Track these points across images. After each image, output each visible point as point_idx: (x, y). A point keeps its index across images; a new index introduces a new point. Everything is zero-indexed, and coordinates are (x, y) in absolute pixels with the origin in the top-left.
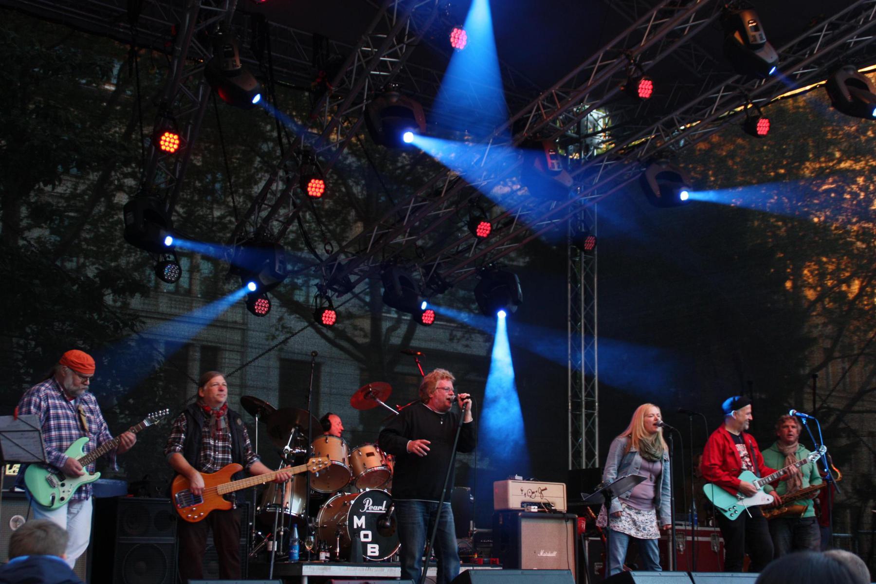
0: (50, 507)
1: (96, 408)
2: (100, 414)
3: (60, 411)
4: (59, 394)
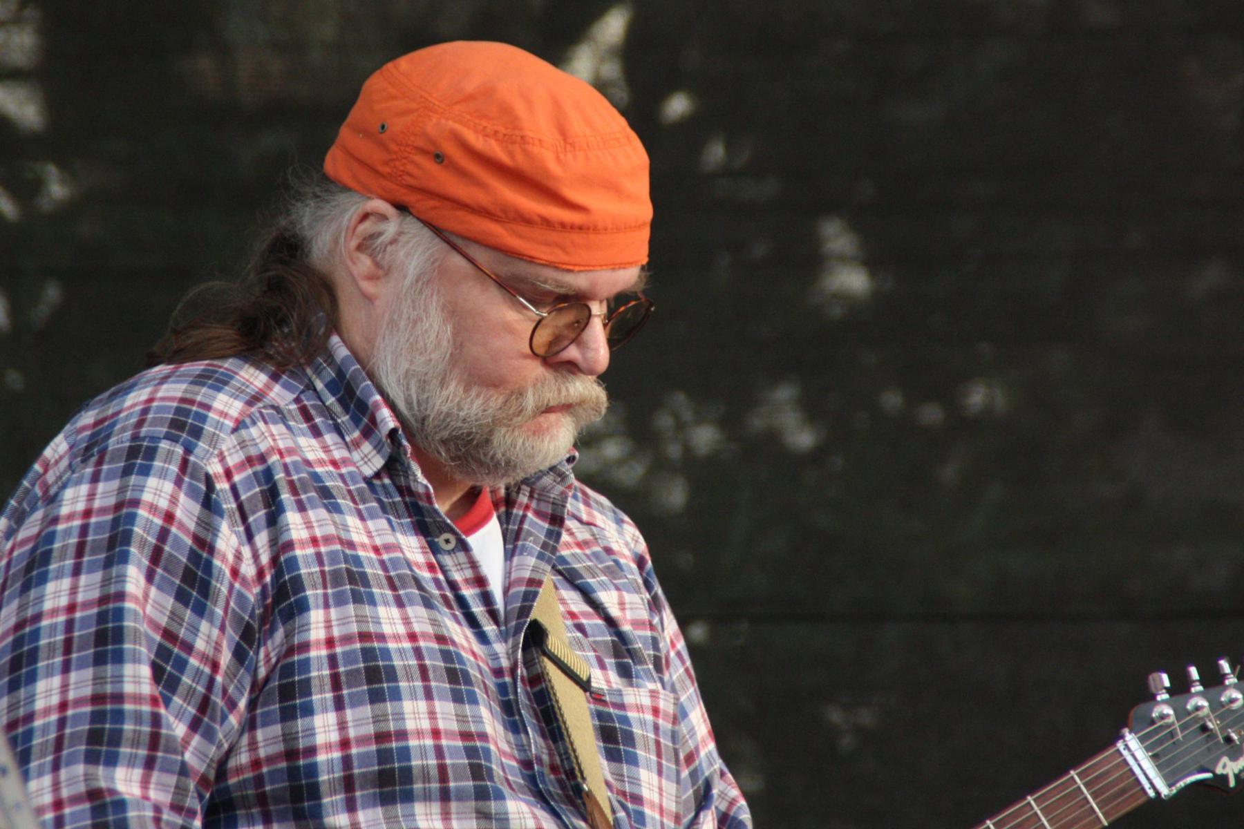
3: (388, 619)
4: (370, 461)
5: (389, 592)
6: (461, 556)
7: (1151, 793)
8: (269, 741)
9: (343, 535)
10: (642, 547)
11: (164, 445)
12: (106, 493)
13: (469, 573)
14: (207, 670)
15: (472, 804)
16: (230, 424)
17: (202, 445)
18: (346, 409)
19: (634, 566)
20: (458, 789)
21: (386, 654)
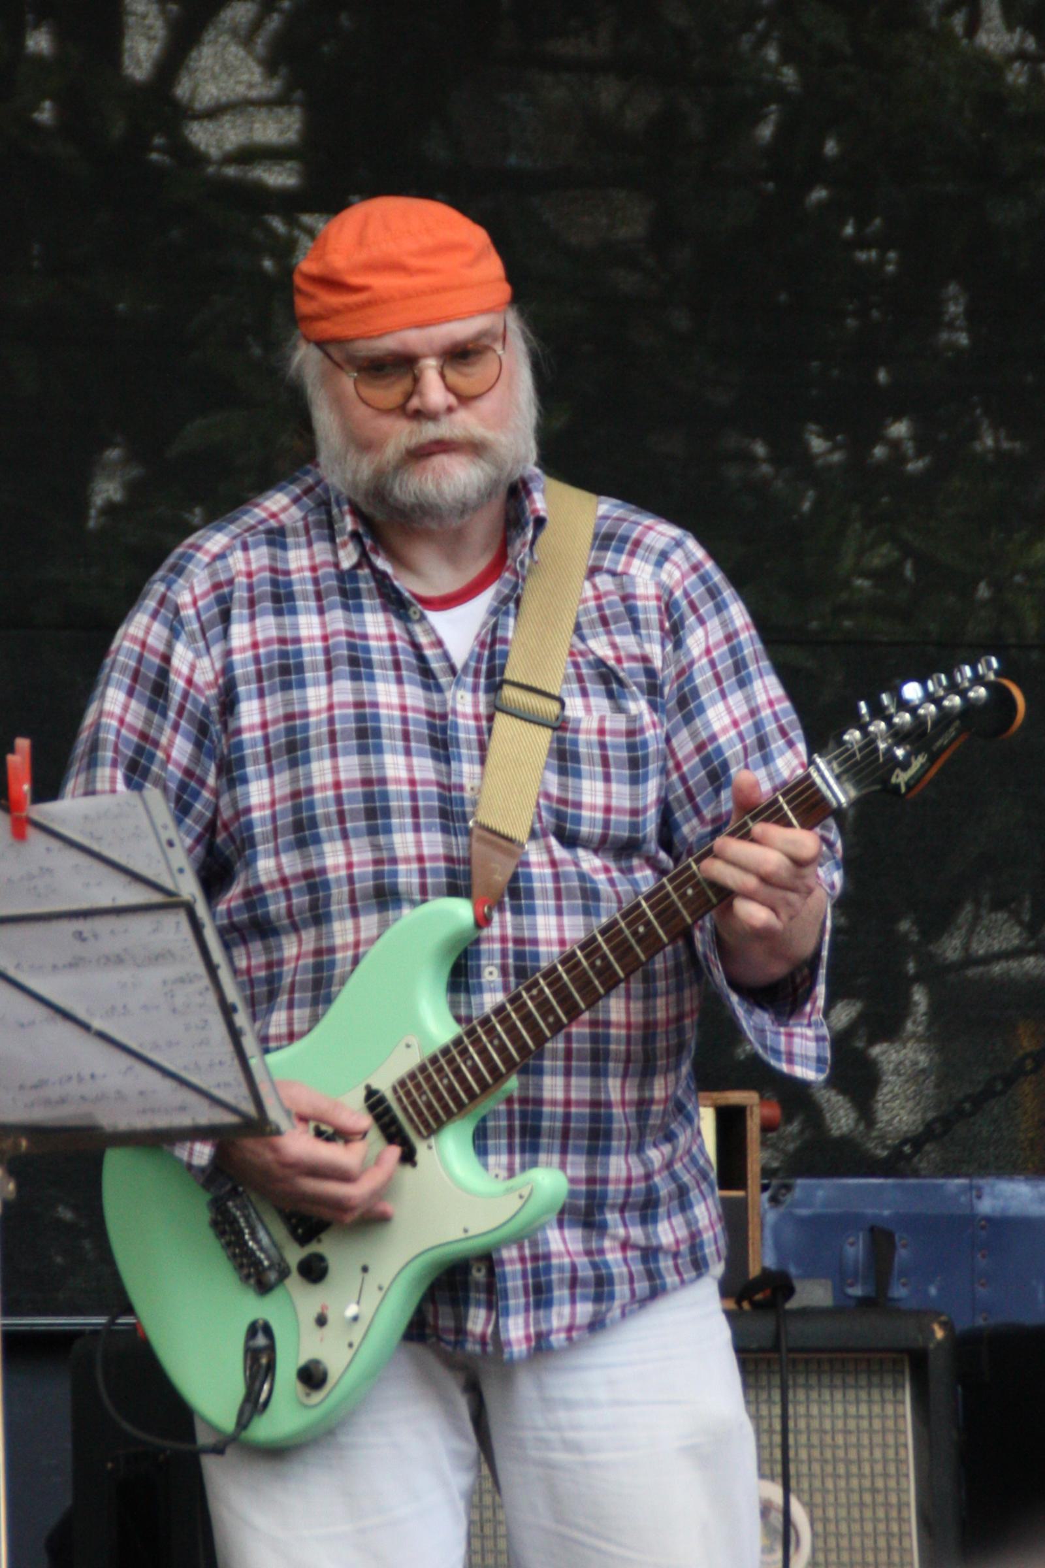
7: (834, 804)
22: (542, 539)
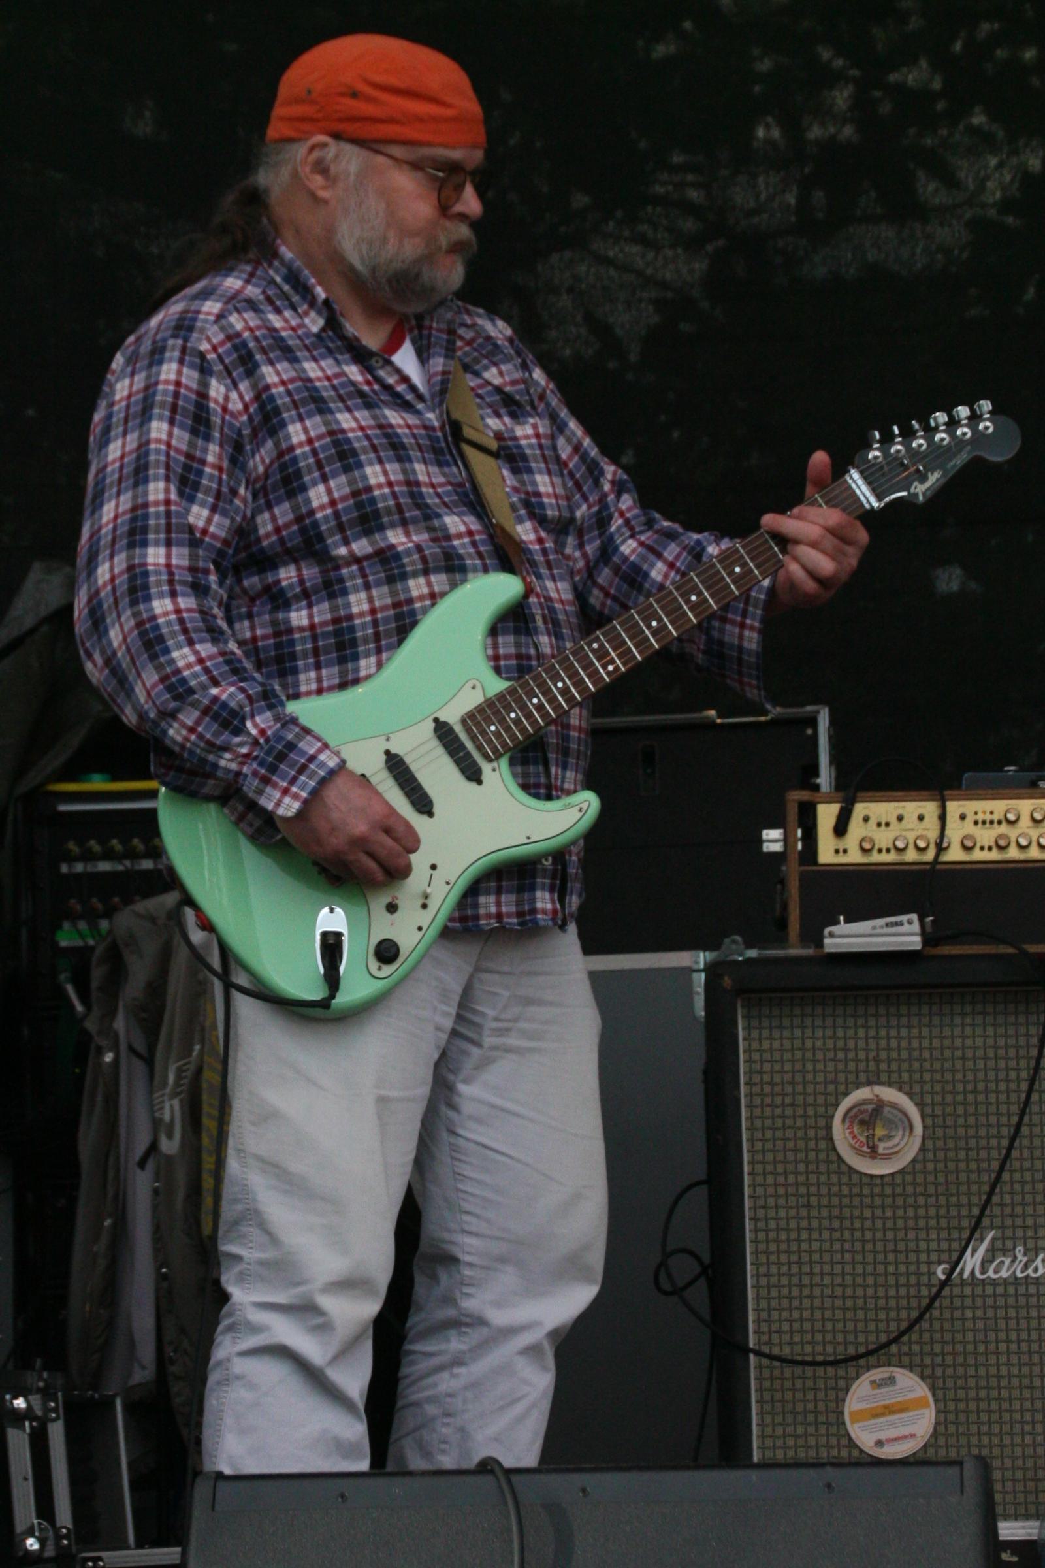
0: (325, 1004)
1: (528, 382)
2: (564, 413)
4: (315, 323)
5: (340, 405)
6: (389, 368)
8: (284, 514)
9: (303, 375)
10: (509, 332)
11: (171, 342)
12: (140, 380)
13: (396, 377)
14: (216, 473)
15: (423, 524)
16: (212, 318)
17: (195, 335)
18: (297, 292)
19: (507, 344)
20: (411, 517)
21: (348, 441)
22: (314, 697)
